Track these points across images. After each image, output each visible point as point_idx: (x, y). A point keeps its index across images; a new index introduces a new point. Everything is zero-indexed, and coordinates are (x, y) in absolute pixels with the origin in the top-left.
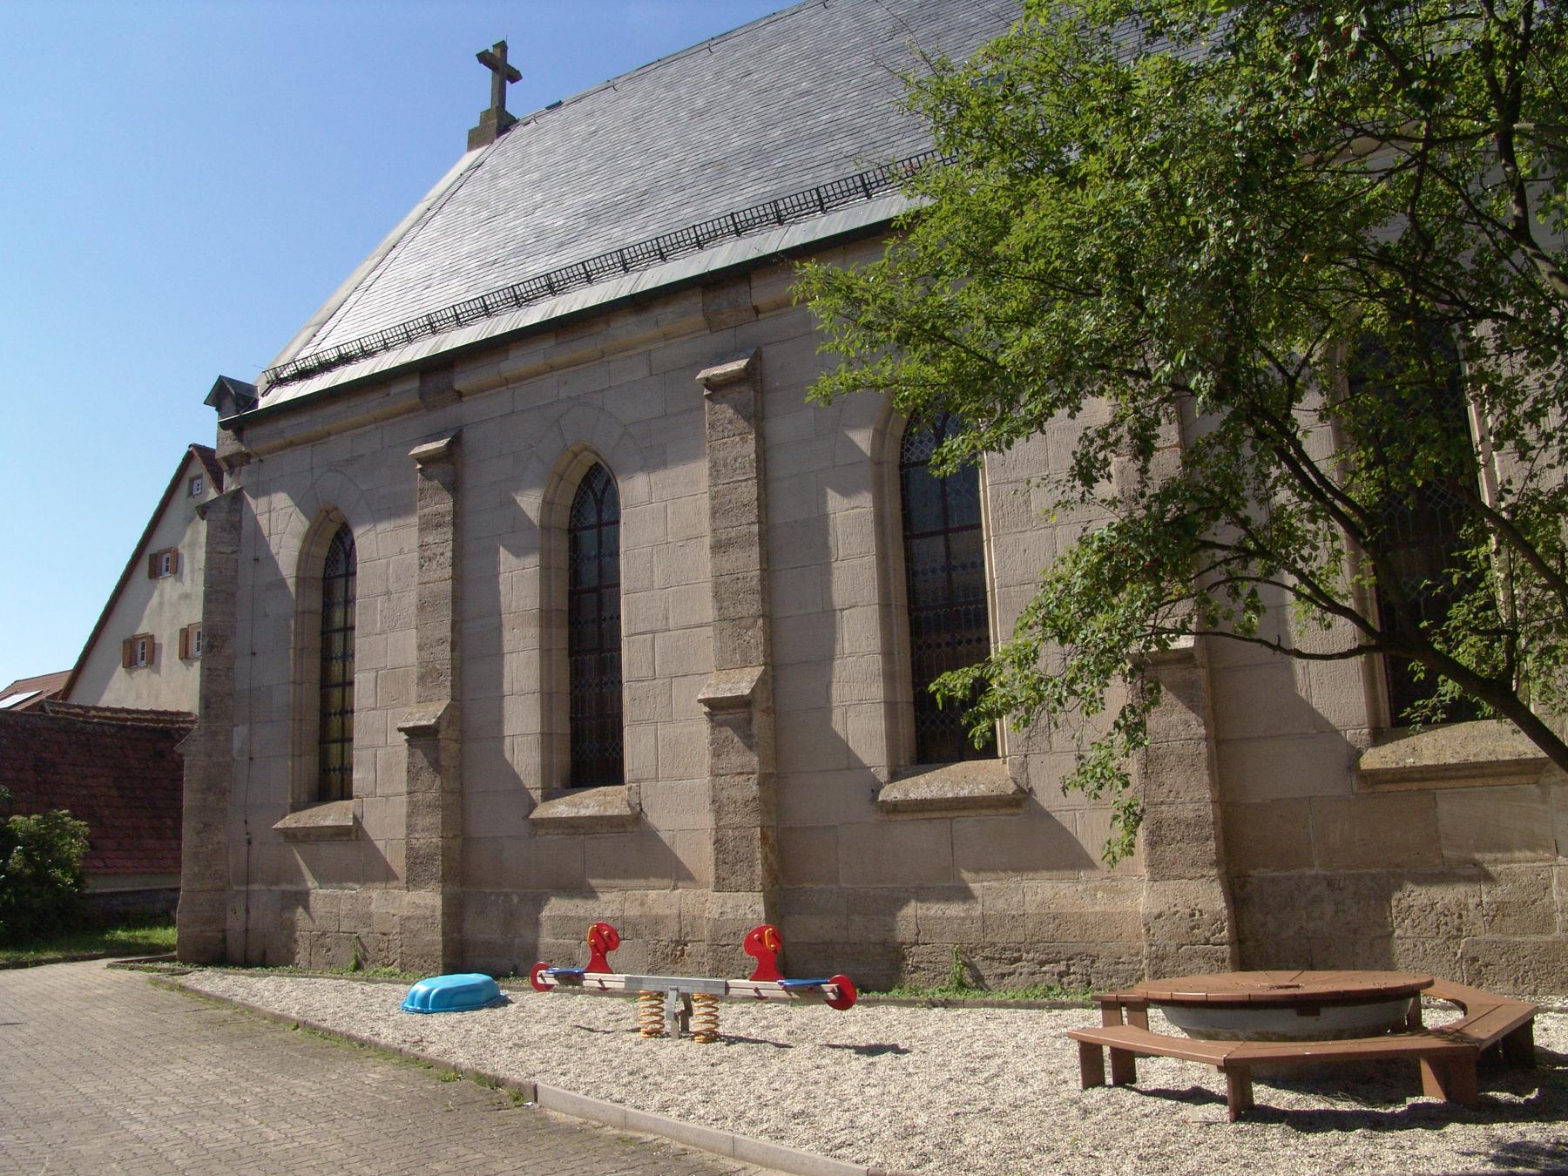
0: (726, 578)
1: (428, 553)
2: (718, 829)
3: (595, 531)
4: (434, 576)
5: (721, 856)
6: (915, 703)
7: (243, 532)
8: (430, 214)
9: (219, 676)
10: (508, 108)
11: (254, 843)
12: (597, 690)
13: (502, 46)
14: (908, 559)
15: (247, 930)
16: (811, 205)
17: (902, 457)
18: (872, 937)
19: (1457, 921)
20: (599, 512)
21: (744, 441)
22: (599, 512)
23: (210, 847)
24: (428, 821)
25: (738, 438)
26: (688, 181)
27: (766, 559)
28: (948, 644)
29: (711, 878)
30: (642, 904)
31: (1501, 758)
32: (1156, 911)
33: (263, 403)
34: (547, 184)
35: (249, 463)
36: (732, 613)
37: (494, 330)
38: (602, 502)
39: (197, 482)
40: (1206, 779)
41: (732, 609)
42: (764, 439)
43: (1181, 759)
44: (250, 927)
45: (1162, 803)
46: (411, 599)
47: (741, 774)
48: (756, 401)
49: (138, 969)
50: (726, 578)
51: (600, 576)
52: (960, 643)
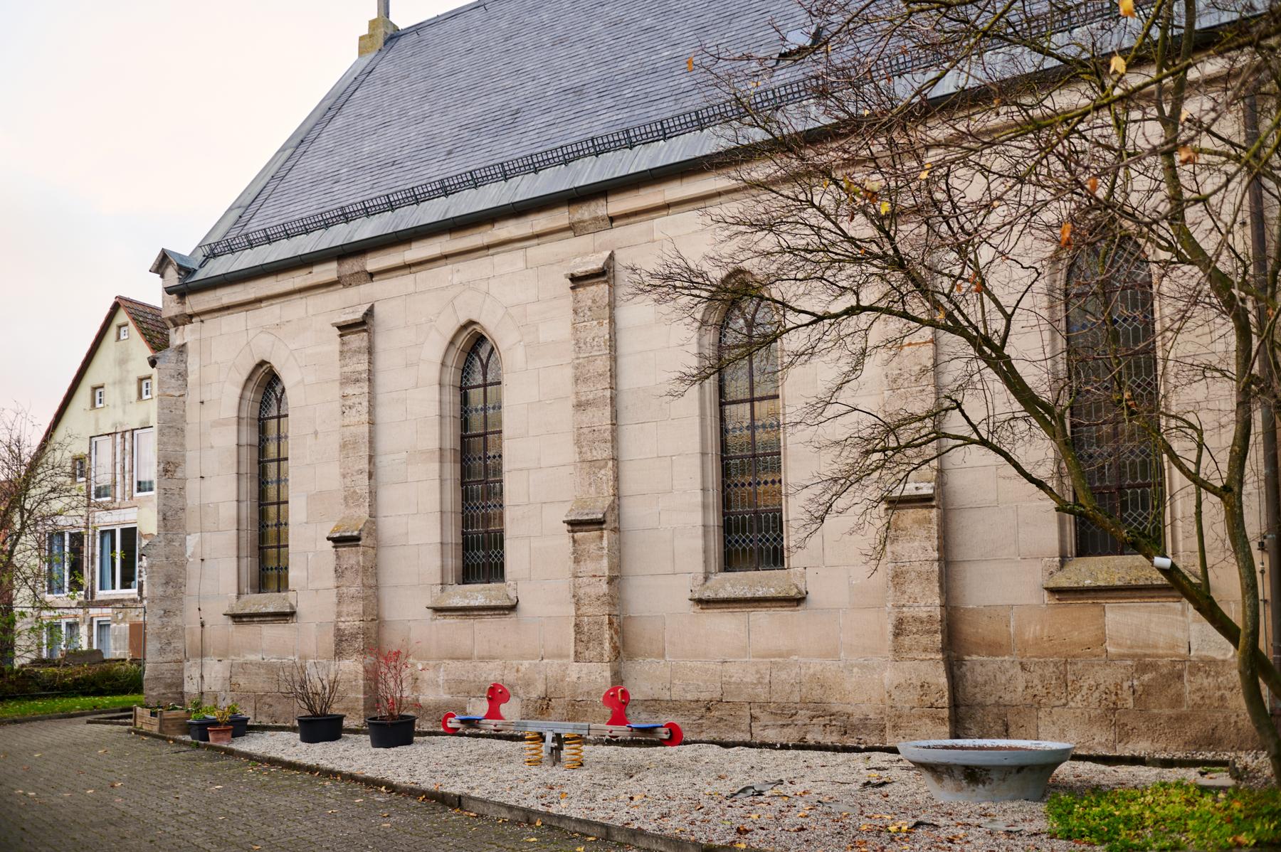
1: (349, 403)
2: (577, 616)
4: (355, 420)
6: (724, 527)
7: (189, 379)
8: (331, 114)
9: (173, 494)
10: (391, 19)
11: (207, 626)
14: (722, 419)
15: (202, 693)
16: (655, 134)
17: (720, 341)
18: (689, 697)
19: (1114, 698)
20: (485, 375)
21: (601, 324)
22: (485, 375)
23: (170, 629)
24: (351, 608)
25: (595, 323)
26: (553, 103)
27: (615, 416)
28: (750, 484)
29: (572, 653)
30: (518, 671)
31: (1155, 583)
32: (896, 683)
33: (200, 275)
34: (432, 96)
36: (589, 457)
37: (397, 226)
39: (123, 329)
40: (937, 590)
43: (919, 574)
45: (904, 606)
46: (334, 441)
47: (595, 576)
52: (759, 483)
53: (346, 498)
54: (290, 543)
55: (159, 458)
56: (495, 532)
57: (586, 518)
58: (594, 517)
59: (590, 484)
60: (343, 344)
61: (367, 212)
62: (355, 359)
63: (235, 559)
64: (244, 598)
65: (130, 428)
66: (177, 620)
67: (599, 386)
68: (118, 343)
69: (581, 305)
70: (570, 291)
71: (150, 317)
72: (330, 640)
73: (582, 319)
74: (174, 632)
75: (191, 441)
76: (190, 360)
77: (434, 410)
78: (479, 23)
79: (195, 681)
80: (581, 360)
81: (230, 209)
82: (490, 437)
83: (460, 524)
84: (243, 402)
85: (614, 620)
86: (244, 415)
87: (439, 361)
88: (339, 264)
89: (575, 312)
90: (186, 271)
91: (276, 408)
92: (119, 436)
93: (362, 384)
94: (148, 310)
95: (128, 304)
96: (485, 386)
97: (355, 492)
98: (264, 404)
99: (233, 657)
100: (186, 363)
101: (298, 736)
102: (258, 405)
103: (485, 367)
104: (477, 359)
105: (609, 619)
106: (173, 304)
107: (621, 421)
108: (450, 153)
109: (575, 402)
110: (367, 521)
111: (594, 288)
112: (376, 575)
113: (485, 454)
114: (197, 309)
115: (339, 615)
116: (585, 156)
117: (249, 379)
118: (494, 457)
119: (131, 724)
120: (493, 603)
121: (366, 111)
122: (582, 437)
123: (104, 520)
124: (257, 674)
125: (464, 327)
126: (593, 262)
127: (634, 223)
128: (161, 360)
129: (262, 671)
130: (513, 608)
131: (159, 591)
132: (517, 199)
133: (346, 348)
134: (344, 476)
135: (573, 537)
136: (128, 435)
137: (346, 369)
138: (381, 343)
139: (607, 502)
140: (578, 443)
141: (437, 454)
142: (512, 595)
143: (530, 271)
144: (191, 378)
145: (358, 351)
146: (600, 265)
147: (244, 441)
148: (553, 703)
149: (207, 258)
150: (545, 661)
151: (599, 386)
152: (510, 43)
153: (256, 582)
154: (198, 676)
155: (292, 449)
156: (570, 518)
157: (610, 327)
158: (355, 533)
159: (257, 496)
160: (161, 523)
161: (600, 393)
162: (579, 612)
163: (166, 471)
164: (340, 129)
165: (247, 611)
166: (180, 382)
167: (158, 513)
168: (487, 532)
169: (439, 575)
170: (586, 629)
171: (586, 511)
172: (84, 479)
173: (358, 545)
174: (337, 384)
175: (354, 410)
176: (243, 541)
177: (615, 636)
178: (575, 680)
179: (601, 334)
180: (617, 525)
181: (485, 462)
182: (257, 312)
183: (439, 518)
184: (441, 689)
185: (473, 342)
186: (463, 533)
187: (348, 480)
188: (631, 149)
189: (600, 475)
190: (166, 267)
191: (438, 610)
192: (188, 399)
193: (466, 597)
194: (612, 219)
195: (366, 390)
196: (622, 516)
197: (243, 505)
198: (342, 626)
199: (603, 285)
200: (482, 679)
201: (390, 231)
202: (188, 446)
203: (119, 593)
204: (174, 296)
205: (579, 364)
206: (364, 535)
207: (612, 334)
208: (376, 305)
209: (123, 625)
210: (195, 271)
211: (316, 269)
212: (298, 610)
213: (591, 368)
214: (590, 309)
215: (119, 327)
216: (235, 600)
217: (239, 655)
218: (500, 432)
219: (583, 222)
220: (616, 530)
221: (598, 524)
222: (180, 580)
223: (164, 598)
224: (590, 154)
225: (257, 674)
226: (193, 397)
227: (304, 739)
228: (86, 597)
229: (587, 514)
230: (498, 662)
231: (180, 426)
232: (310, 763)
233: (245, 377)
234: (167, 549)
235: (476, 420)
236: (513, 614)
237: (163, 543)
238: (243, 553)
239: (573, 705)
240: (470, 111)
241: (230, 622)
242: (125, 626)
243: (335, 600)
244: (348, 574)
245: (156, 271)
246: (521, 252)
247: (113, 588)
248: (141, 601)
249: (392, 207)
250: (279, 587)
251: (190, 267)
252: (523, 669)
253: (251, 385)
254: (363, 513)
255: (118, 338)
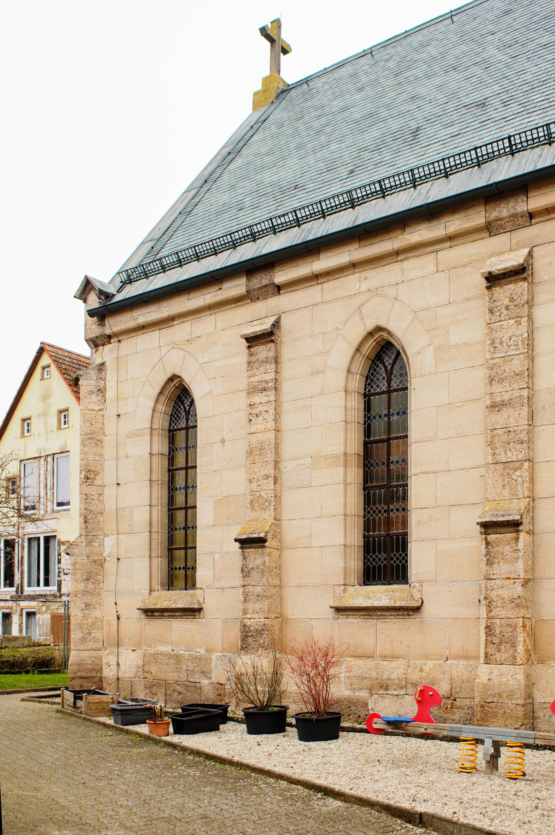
0: (499, 432)
1: (256, 411)
2: (489, 618)
3: (384, 397)
4: (260, 427)
5: (489, 639)
9: (93, 499)
12: (386, 515)
13: (277, 23)
15: (118, 679)
17: (170, 426)
20: (389, 381)
22: (389, 381)
23: (90, 620)
24: (257, 606)
25: (512, 321)
27: (532, 416)
29: (482, 654)
30: (421, 670)
33: (119, 298)
34: (328, 130)
35: (109, 343)
38: (391, 373)
39: (46, 370)
41: (503, 455)
42: (533, 323)
44: (120, 677)
46: (241, 448)
47: (509, 578)
48: (528, 291)
49: (45, 702)
50: (499, 432)
51: (389, 430)
53: (251, 502)
54: (198, 545)
55: (81, 467)
56: (397, 535)
57: (501, 519)
58: (511, 518)
59: (504, 486)
60: (251, 355)
61: (274, 230)
62: (262, 369)
63: (148, 559)
64: (155, 594)
65: (51, 453)
66: (96, 613)
67: (515, 386)
68: (42, 381)
69: (497, 304)
70: (486, 291)
71: (67, 359)
72: (235, 634)
73: (499, 319)
74: (93, 624)
75: (109, 451)
76: (108, 377)
77: (339, 415)
78: (367, 67)
79: (112, 667)
80: (496, 361)
81: (143, 243)
82: (394, 442)
83: (362, 527)
84: (156, 414)
85: (527, 623)
86: (155, 426)
87: (346, 368)
88: (248, 279)
89: (491, 311)
90: (105, 295)
91: (184, 420)
92: (42, 460)
93: (268, 393)
94: (66, 354)
95: (50, 349)
96: (389, 392)
97: (260, 496)
98: (174, 417)
99: (145, 648)
100: (105, 380)
101: (244, 726)
102: (168, 418)
103: (389, 374)
104: (381, 365)
105: (523, 623)
106: (94, 327)
107: (538, 421)
108: (352, 172)
109: (488, 402)
110: (273, 524)
111: (512, 286)
112: (279, 575)
113: (388, 459)
114: (116, 329)
115: (245, 612)
116: (500, 156)
117: (161, 393)
118: (397, 462)
119: (59, 704)
120: (398, 604)
121: (264, 150)
122: (496, 438)
123: (30, 529)
124: (167, 664)
125: (371, 334)
126: (512, 259)
127: (203, 316)
128: (84, 377)
129: (172, 661)
130: (417, 609)
131: (81, 586)
132: (430, 201)
133: (253, 359)
134: (250, 481)
135: (486, 539)
136: (50, 459)
137: (253, 379)
138: (286, 352)
139: (523, 503)
140: (491, 444)
141: (342, 459)
142: (417, 596)
143: (442, 274)
144: (110, 394)
145: (266, 361)
146: (521, 261)
147: (155, 451)
148: (458, 703)
149: (124, 283)
150: (450, 662)
151: (515, 386)
152: (400, 78)
153: (166, 581)
154: (114, 663)
155: (201, 457)
156: (484, 520)
157: (529, 325)
158: (262, 535)
159: (166, 502)
160: (83, 525)
161: (517, 393)
162: (492, 614)
163: (87, 478)
164: (240, 168)
165: (158, 606)
166: (99, 398)
167: (80, 516)
168: (388, 535)
169: (342, 576)
170: (498, 632)
171: (501, 513)
172: (15, 495)
173: (264, 547)
174: (245, 393)
175: (261, 418)
176: (154, 542)
177: (527, 639)
178: (486, 681)
179: (518, 333)
180: (531, 527)
181: (388, 467)
182: (169, 330)
183: (343, 522)
184: (342, 685)
185: (378, 350)
186: (365, 537)
187: (254, 486)
188: (550, 144)
189: (514, 477)
190: (89, 293)
191: (339, 610)
192: (107, 413)
193: (370, 598)
194: (531, 216)
195: (272, 398)
196: (537, 519)
197: (155, 510)
198: (248, 622)
199: (521, 283)
200: (385, 677)
201: (299, 242)
202: (106, 456)
203: (42, 589)
204: (95, 319)
205: (494, 364)
206: (269, 537)
207: (530, 332)
208: (282, 316)
209: (45, 616)
210: (114, 295)
211: (226, 285)
212: (204, 606)
213: (507, 368)
214: (507, 308)
215: (44, 368)
216: (147, 597)
217: (151, 646)
218: (406, 437)
219: (501, 219)
220: (530, 532)
221: (515, 525)
222: (99, 577)
223: (85, 592)
224: (506, 154)
225: (167, 664)
226: (111, 410)
227: (251, 731)
228: (17, 591)
229: (503, 516)
230: (400, 661)
231: (99, 438)
232: (432, 812)
233: (157, 391)
234: (88, 549)
235: (379, 425)
236: (418, 616)
237: (84, 544)
238: (154, 554)
239: (482, 706)
240: (367, 136)
241: (143, 616)
242: (48, 616)
243: (241, 598)
244: (254, 574)
245: (80, 297)
246: (433, 256)
247: (38, 585)
248: (60, 596)
249: (298, 223)
250: (186, 585)
251: (110, 292)
252: (426, 668)
253: (163, 399)
254: (268, 516)
255: (42, 379)
